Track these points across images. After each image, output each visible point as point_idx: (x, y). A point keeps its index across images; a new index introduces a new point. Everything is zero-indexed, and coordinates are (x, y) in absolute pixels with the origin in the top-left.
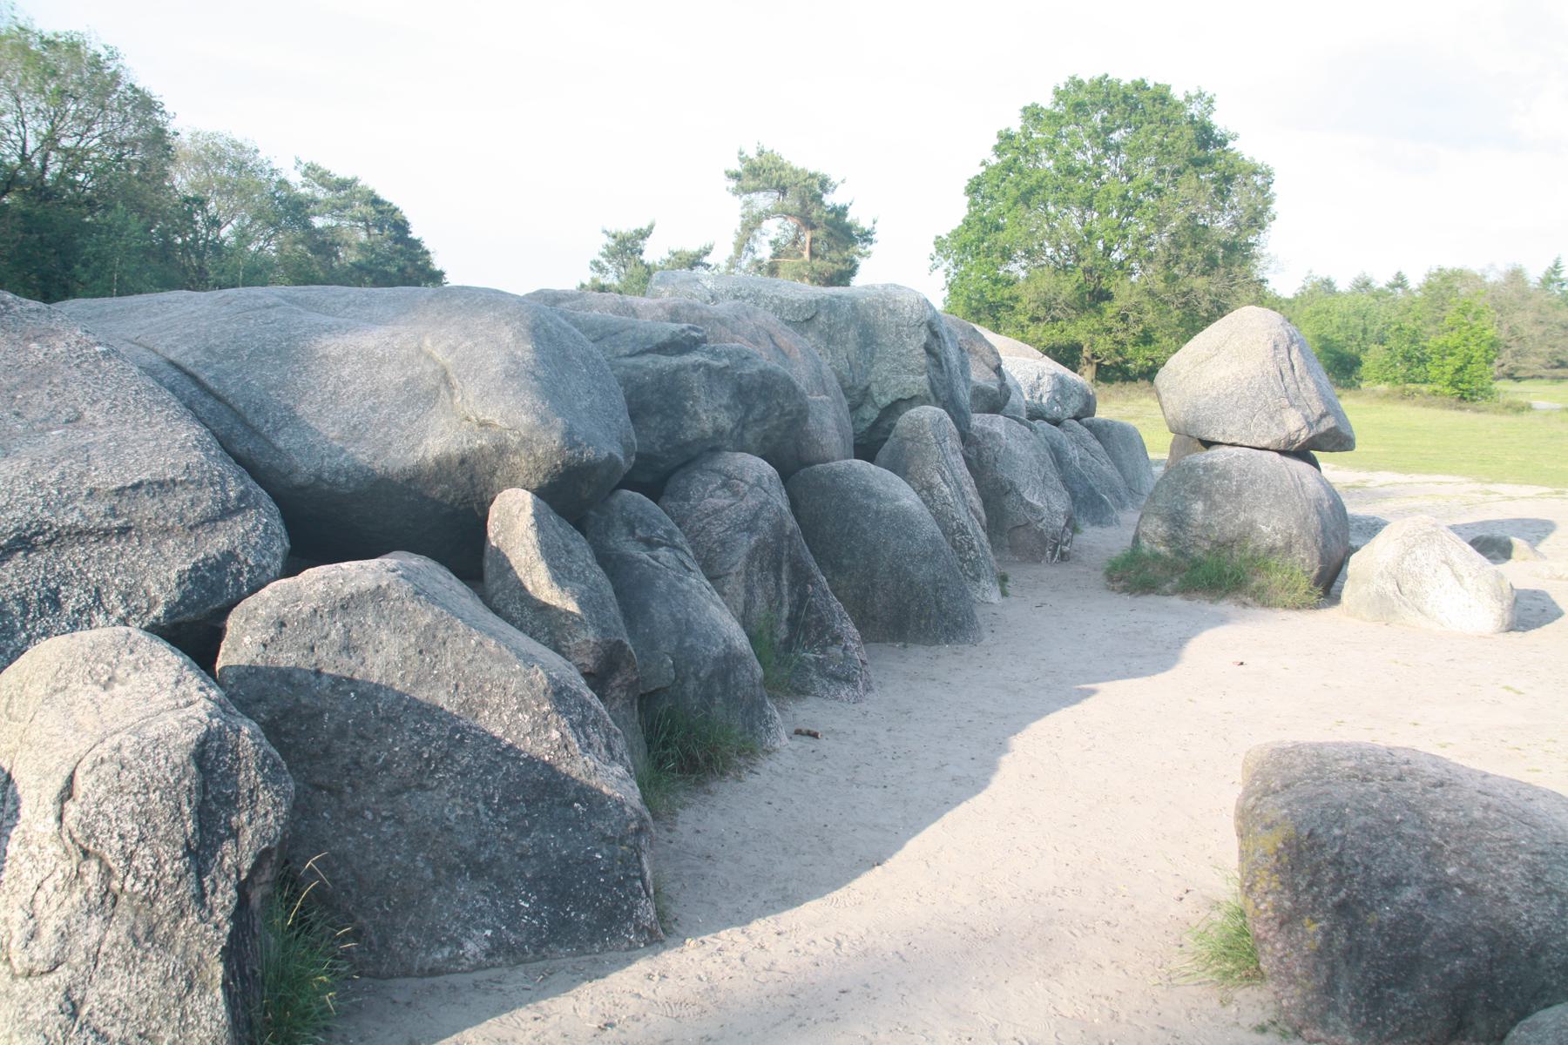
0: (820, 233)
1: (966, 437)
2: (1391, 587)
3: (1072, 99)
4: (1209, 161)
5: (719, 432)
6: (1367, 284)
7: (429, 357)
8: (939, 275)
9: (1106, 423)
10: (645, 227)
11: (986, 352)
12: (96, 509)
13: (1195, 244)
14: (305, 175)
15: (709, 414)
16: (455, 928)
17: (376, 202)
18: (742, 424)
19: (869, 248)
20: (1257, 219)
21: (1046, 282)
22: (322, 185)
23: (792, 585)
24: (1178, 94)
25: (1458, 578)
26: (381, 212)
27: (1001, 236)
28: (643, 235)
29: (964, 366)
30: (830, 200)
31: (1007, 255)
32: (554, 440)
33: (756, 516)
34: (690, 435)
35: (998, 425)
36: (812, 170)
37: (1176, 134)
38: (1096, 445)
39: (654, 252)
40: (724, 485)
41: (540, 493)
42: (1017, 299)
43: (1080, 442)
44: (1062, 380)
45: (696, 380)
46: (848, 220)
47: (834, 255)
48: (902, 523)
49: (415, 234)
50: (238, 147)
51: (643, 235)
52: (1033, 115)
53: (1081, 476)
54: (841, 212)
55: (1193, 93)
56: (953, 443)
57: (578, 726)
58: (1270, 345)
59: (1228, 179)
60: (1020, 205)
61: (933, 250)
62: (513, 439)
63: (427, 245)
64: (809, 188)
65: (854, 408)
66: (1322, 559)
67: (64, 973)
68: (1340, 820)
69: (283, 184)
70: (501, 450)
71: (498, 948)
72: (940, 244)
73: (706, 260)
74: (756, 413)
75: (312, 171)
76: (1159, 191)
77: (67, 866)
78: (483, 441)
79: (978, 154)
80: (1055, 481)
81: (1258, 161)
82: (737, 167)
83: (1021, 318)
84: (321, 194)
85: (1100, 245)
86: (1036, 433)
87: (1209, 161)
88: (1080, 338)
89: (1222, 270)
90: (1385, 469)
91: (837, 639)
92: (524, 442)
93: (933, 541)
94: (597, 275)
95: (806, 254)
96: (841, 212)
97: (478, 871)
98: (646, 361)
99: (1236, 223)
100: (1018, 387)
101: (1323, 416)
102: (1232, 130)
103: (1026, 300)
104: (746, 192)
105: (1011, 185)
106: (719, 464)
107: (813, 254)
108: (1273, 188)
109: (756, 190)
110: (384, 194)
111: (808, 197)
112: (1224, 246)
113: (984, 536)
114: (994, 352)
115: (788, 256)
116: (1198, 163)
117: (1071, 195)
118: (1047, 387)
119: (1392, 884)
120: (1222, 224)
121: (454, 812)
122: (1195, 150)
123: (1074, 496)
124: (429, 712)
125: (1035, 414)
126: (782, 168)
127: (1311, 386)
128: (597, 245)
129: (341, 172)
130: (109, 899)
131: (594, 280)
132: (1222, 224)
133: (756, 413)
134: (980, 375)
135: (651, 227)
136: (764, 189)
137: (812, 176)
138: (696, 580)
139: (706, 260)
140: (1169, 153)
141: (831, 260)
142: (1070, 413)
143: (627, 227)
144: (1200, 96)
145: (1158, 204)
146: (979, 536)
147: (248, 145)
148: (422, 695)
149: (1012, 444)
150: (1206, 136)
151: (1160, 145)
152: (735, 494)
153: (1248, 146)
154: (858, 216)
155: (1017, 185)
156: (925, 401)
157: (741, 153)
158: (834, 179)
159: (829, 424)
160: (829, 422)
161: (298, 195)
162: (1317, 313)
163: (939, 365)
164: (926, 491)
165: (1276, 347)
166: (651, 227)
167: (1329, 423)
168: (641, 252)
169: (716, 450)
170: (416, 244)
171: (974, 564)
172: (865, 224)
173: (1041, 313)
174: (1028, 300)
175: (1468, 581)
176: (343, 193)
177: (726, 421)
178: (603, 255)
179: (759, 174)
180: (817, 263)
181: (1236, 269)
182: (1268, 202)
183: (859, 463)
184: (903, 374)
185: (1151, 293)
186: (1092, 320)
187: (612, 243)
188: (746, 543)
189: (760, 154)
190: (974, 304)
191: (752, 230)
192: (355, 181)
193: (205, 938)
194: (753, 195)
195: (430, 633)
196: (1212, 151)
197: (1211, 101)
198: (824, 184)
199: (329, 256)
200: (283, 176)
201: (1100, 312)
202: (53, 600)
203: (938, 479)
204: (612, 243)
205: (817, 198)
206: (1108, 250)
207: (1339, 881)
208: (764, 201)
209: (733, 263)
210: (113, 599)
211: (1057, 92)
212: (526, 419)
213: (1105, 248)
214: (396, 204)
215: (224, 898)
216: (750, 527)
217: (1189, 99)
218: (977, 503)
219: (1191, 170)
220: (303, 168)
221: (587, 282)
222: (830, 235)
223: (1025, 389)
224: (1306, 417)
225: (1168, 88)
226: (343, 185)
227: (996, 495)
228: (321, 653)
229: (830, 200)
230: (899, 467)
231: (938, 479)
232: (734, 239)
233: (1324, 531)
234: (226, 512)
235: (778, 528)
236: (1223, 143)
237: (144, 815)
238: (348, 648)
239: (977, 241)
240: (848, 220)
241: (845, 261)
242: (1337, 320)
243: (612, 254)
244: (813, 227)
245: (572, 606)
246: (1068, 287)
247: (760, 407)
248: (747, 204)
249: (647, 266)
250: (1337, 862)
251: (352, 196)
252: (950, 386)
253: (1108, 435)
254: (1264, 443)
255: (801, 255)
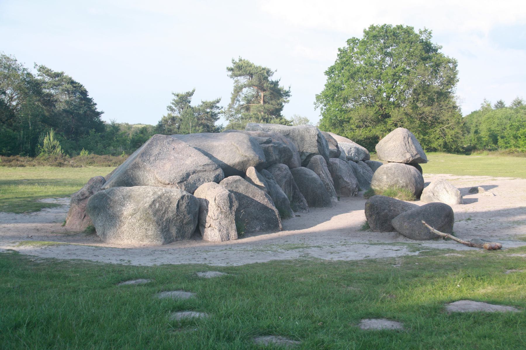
0: (267, 93)
1: (328, 163)
2: (431, 194)
3: (372, 34)
4: (430, 58)
5: (276, 159)
6: (519, 103)
7: (234, 145)
8: (319, 110)
9: (373, 162)
10: (191, 91)
11: (333, 141)
12: (201, 168)
13: (424, 93)
14: (39, 71)
15: (275, 156)
16: (255, 227)
17: (72, 82)
18: (280, 158)
19: (289, 99)
20: (451, 81)
21: (363, 111)
22: (48, 75)
23: (293, 190)
24: (416, 31)
25: (447, 191)
26: (75, 87)
27: (343, 92)
28: (190, 94)
29: (327, 146)
30: (272, 79)
31: (346, 100)
32: (257, 158)
33: (286, 175)
34: (271, 160)
35: (337, 161)
36: (263, 67)
37: (415, 48)
38: (369, 168)
39: (195, 102)
40: (279, 170)
41: (256, 167)
42: (350, 118)
43: (364, 167)
44: (358, 149)
45: (271, 149)
46: (279, 87)
47: (273, 102)
48: (314, 180)
49: (90, 96)
50: (8, 59)
51: (190, 94)
52: (353, 41)
53: (362, 176)
54: (276, 84)
55: (423, 30)
56: (325, 164)
57: (269, 200)
58: (403, 137)
59: (438, 65)
60: (350, 80)
61: (315, 101)
62: (250, 158)
63: (95, 101)
64: (262, 74)
65: (301, 156)
66: (416, 189)
67: (218, 220)
68: (377, 202)
69: (29, 74)
70: (249, 160)
71: (261, 229)
72: (318, 98)
73: (218, 105)
74: (283, 156)
75: (42, 69)
76: (408, 71)
77: (217, 208)
78: (246, 159)
79: (332, 59)
80: (353, 175)
81: (451, 58)
82: (231, 66)
83: (353, 126)
84: (47, 79)
85: (384, 95)
86: (348, 163)
87: (430, 58)
88: (377, 134)
89: (437, 103)
90: (468, 175)
91: (302, 201)
92: (252, 159)
93: (321, 184)
94: (170, 112)
95: (262, 102)
96: (276, 84)
97: (257, 219)
98: (262, 145)
99: (442, 84)
100: (344, 151)
101: (416, 154)
102: (439, 44)
103: (354, 119)
104: (236, 76)
105: (345, 71)
106: (277, 166)
107: (264, 102)
108: (457, 68)
109: (240, 75)
110: (76, 79)
111: (262, 78)
112: (437, 93)
113: (333, 187)
114: (336, 141)
115: (254, 103)
116: (424, 59)
117: (372, 75)
118: (353, 151)
119: (384, 210)
120: (436, 84)
121: (253, 211)
122: (423, 53)
123: (359, 181)
124: (248, 197)
125: (349, 159)
126: (251, 66)
127: (414, 147)
128: (170, 100)
129: (56, 69)
130: (221, 212)
131: (169, 115)
132: (436, 84)
133: (283, 156)
134: (332, 148)
135: (194, 91)
136: (243, 75)
137: (264, 69)
138: (277, 185)
139: (218, 105)
140: (412, 56)
141: (272, 104)
142: (361, 159)
143: (183, 91)
144: (426, 31)
145: (408, 77)
146: (332, 187)
147: (12, 58)
148: (247, 195)
149: (341, 166)
150: (428, 48)
151: (408, 52)
152: (281, 171)
153: (447, 51)
154: (283, 85)
155: (349, 71)
156: (318, 154)
157: (233, 60)
158: (273, 70)
159: (296, 160)
160: (296, 159)
161: (37, 80)
162: (489, 118)
163: (321, 145)
164: (319, 175)
165: (404, 138)
166: (194, 91)
167: (418, 156)
168: (189, 102)
169: (275, 163)
170: (90, 100)
171: (331, 193)
172: (286, 89)
173: (361, 124)
174: (355, 117)
175: (449, 192)
176: (57, 79)
177: (277, 157)
178: (173, 104)
179: (240, 69)
180: (267, 105)
181: (442, 103)
182: (455, 74)
183: (303, 168)
184: (311, 147)
185: (406, 114)
186: (382, 126)
187: (176, 98)
188: (284, 180)
189: (240, 60)
190: (333, 121)
191: (238, 92)
192: (62, 73)
193: (233, 217)
194: (239, 78)
195: (247, 186)
196: (431, 54)
197: (430, 33)
198: (268, 72)
199: (51, 106)
200: (29, 71)
201: (385, 123)
202: (199, 180)
203: (321, 172)
204: (176, 98)
205: (266, 79)
206: (388, 97)
207: (377, 210)
208: (243, 80)
209: (230, 106)
210: (206, 180)
211: (365, 31)
212: (252, 155)
213: (387, 96)
214: (81, 83)
215: (234, 213)
216: (285, 177)
217: (421, 32)
218: (331, 179)
219: (421, 62)
220: (38, 68)
221: (166, 115)
222: (272, 93)
223: (346, 152)
224: (411, 155)
225: (413, 28)
226: (57, 75)
227: (337, 179)
228: (233, 188)
229: (270, 79)
230: (312, 168)
231: (321, 172)
232: (231, 96)
233: (416, 182)
234: (217, 169)
235: (290, 177)
236: (436, 50)
237: (224, 202)
238: (236, 187)
239: (332, 95)
240: (279, 87)
241: (278, 104)
242: (497, 121)
243: (177, 103)
244: (264, 90)
245: (263, 185)
246: (371, 113)
247: (284, 155)
248: (236, 81)
249: (192, 108)
250: (376, 207)
251: (62, 80)
252: (324, 150)
253: (374, 165)
254: (401, 161)
255: (260, 102)
